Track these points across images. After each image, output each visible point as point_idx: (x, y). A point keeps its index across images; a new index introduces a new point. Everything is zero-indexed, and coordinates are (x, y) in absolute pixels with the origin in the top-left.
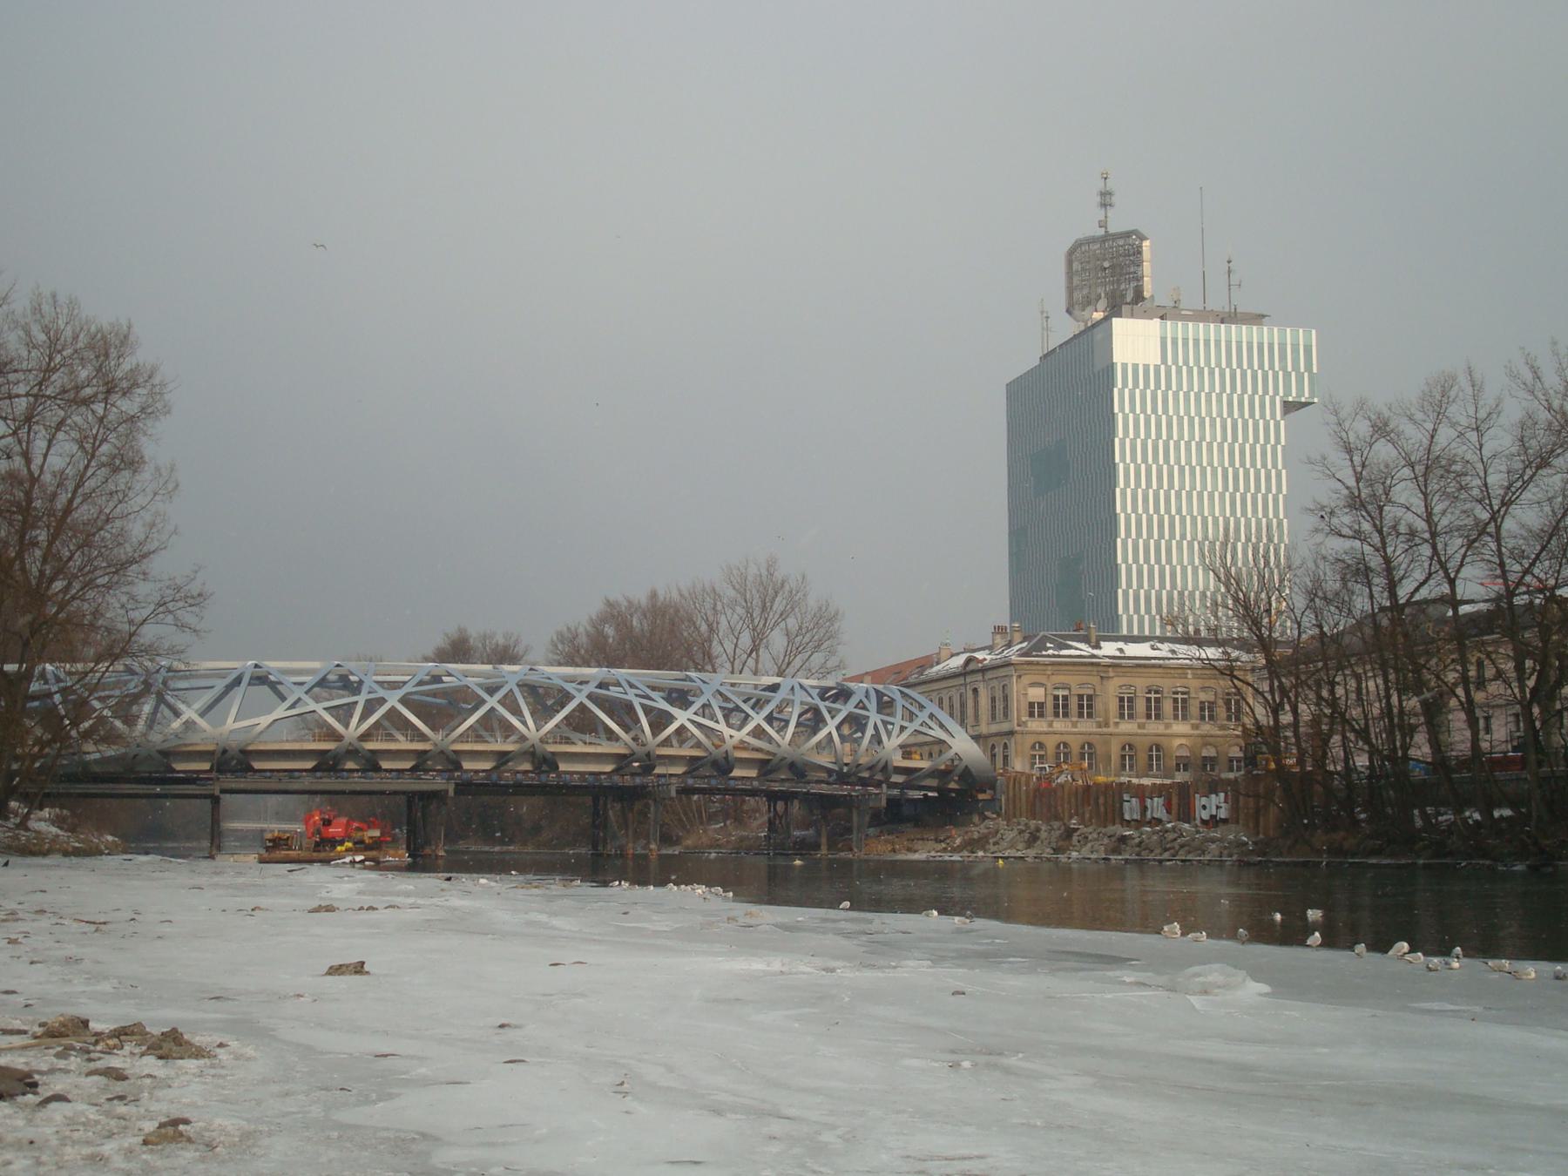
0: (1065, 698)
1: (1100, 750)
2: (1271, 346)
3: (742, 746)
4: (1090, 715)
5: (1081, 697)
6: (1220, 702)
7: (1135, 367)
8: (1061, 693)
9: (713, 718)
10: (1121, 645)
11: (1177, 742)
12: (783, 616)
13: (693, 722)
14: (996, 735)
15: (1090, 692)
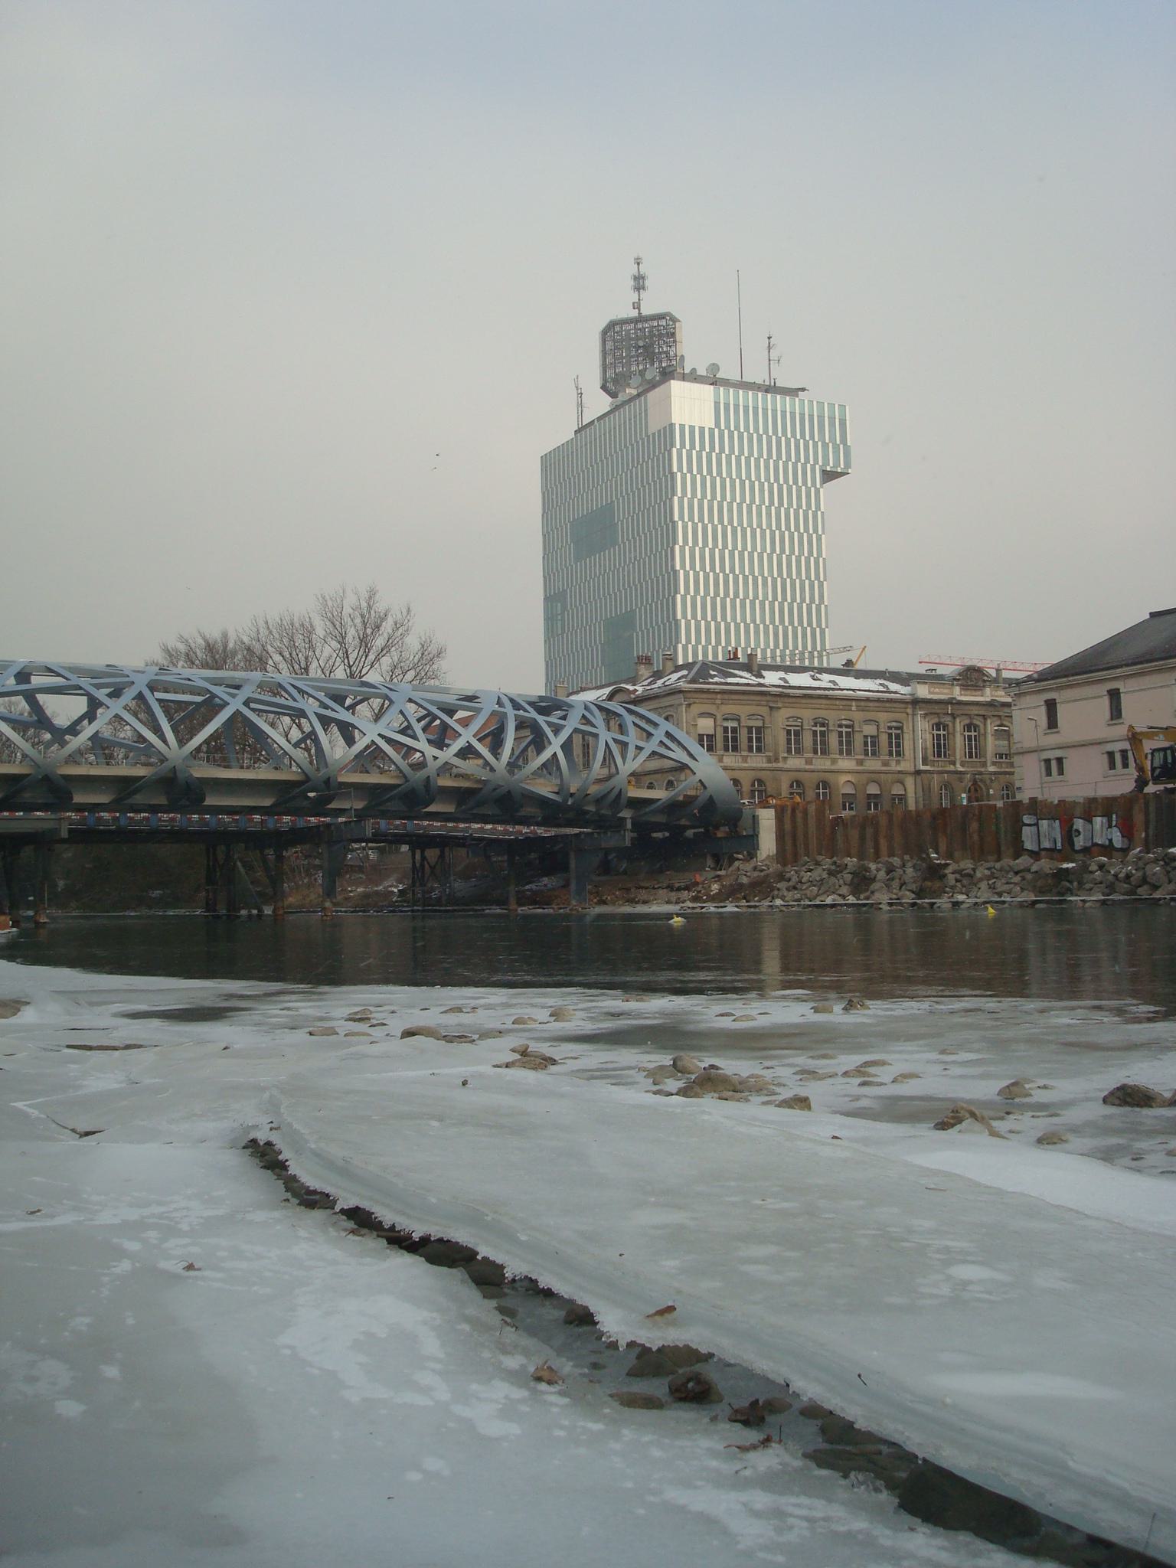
0: (734, 730)
1: (771, 788)
2: (811, 416)
3: (446, 768)
4: (759, 749)
5: (750, 729)
6: (884, 738)
7: (692, 428)
8: (730, 724)
9: (414, 737)
10: (782, 674)
11: (843, 778)
12: (385, 649)
13: (389, 741)
14: (656, 772)
15: (759, 724)
